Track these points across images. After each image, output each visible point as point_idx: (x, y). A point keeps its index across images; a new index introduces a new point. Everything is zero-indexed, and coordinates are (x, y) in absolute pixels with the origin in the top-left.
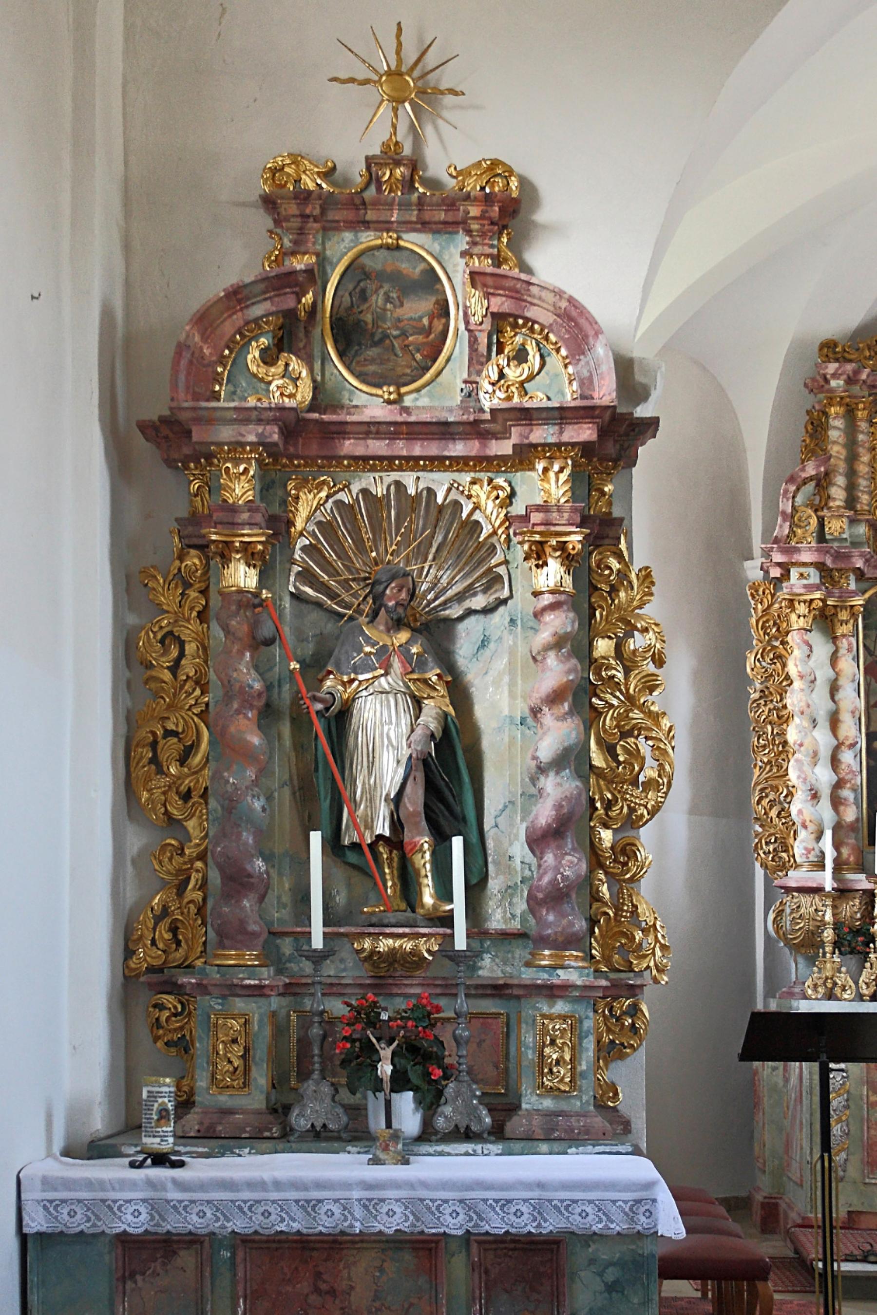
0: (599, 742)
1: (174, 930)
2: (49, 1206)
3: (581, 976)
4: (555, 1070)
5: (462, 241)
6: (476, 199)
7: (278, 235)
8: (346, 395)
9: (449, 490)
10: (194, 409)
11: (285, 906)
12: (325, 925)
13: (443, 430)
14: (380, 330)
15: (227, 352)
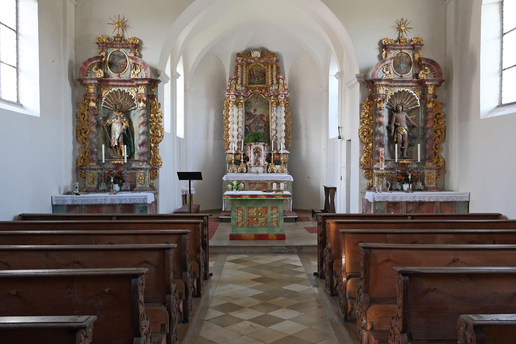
1: (84, 160)
2: (56, 201)
5: (129, 50)
13: (125, 81)
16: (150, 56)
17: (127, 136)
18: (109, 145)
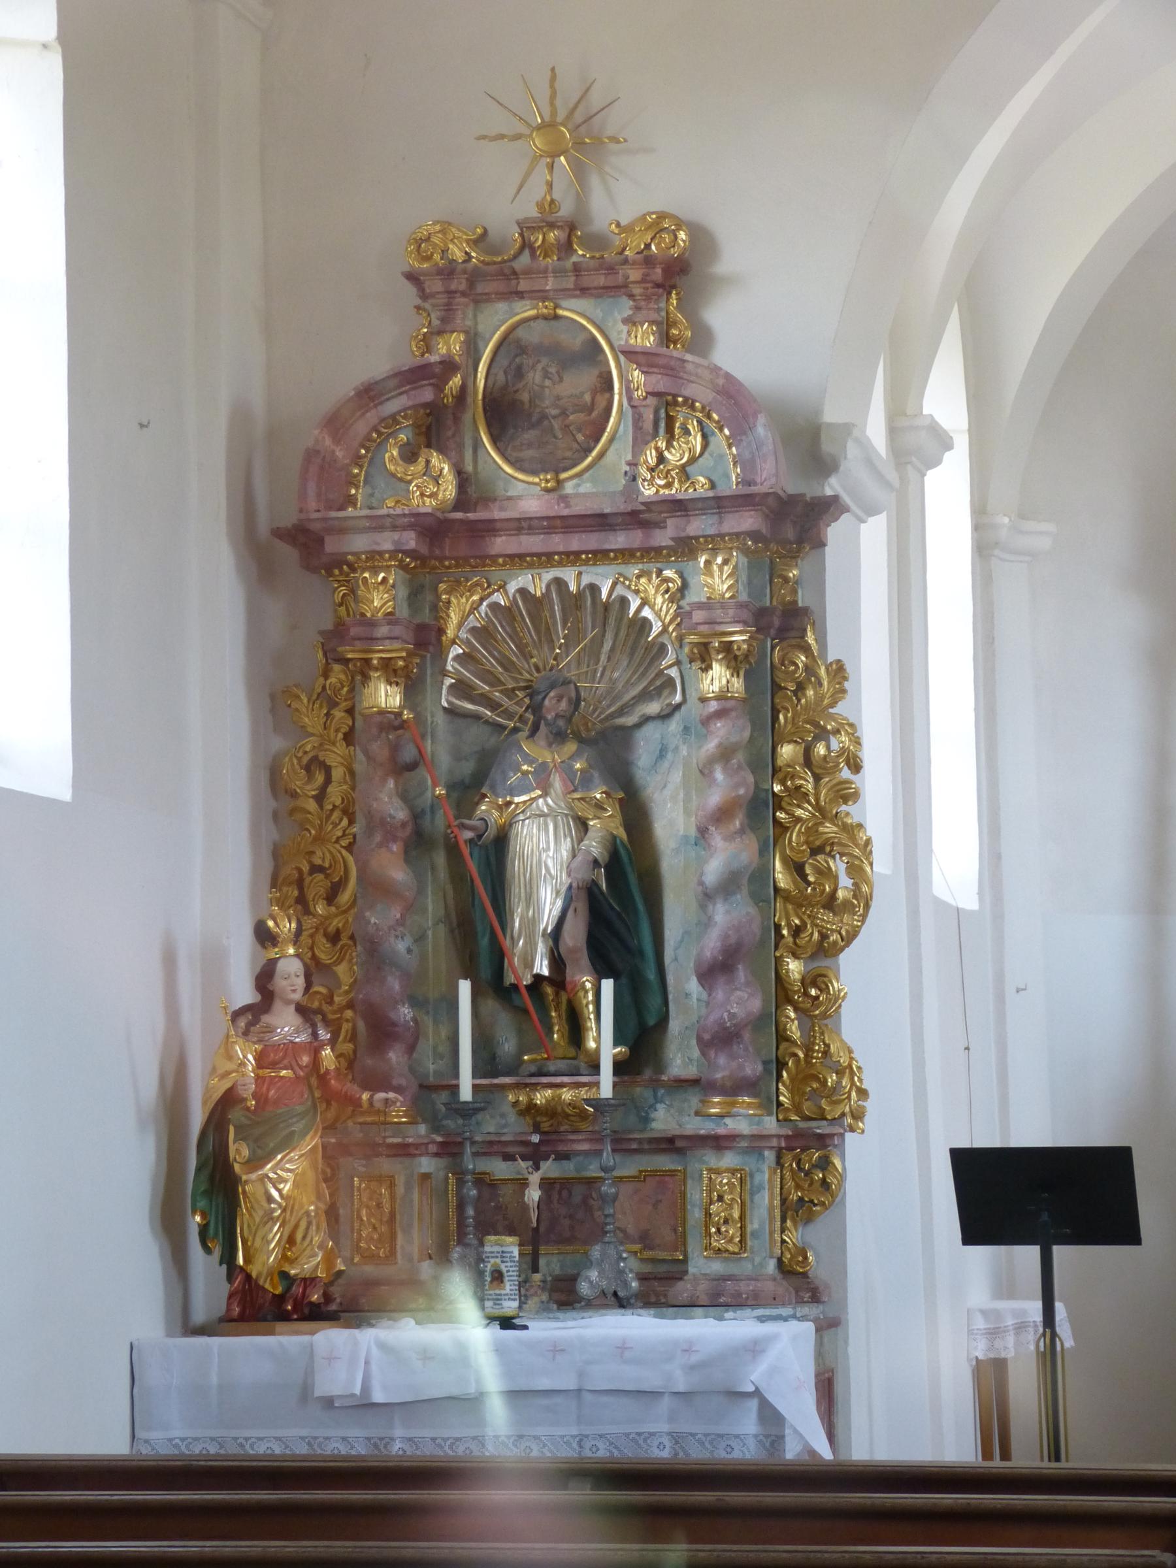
0: (786, 861)
3: (750, 1125)
4: (723, 1229)
5: (625, 307)
6: (634, 263)
7: (425, 310)
8: (501, 484)
9: (614, 584)
10: (325, 519)
11: (442, 1058)
12: (474, 1076)
13: (601, 522)
14: (538, 410)
15: (363, 451)
16: (756, 332)
17: (619, 907)
18: (495, 985)
